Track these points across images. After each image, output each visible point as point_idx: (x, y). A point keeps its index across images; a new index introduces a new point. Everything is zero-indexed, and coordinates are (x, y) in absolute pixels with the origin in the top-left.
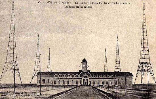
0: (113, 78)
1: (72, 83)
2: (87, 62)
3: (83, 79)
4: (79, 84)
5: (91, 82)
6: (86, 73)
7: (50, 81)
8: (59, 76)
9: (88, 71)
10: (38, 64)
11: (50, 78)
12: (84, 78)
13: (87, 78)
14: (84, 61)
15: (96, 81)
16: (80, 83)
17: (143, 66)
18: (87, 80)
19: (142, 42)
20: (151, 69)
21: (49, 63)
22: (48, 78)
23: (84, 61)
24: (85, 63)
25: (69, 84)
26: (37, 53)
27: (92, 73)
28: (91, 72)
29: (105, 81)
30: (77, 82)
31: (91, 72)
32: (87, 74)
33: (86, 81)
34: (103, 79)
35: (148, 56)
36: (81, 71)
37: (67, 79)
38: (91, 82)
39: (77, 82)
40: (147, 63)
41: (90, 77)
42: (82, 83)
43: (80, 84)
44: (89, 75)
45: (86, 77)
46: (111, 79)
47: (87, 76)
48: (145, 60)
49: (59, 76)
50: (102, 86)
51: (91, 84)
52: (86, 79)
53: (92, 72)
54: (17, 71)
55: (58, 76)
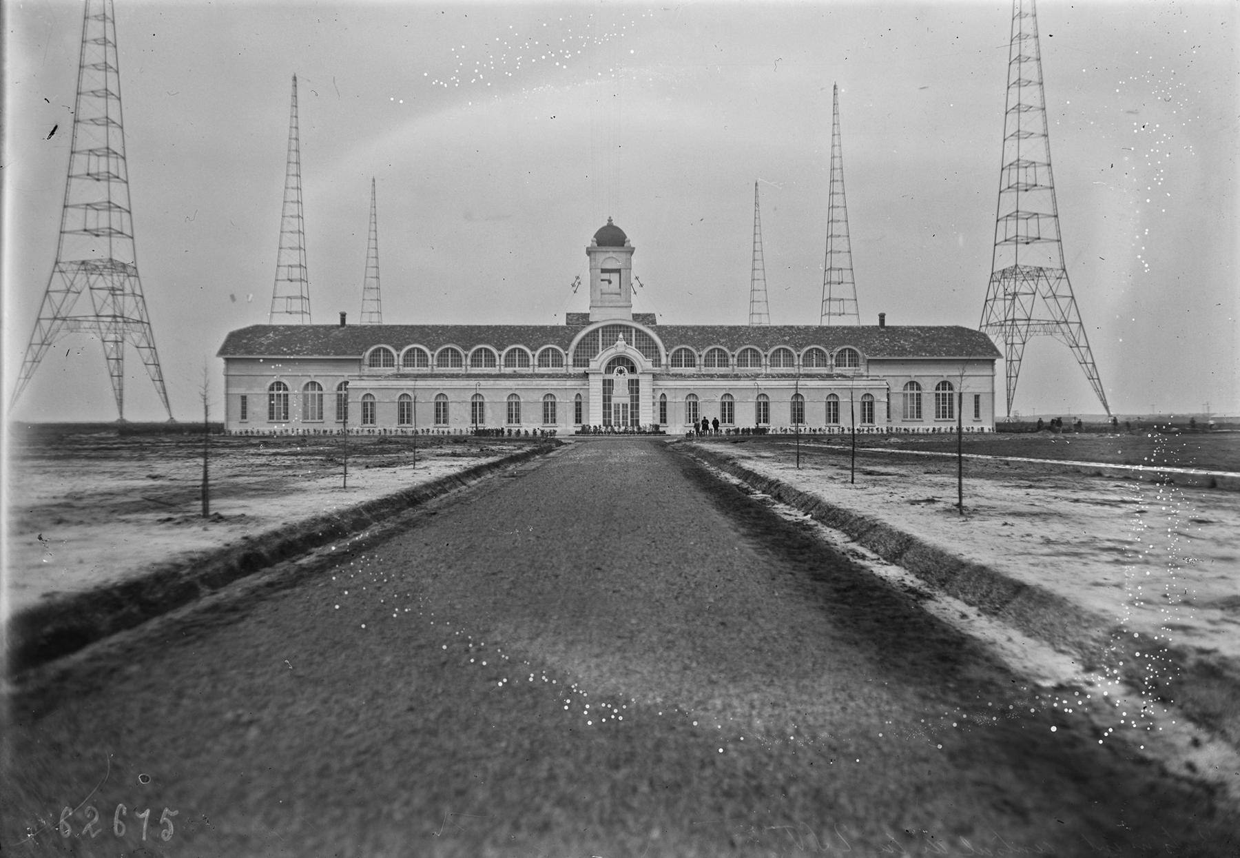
0: (837, 370)
1: (514, 413)
2: (631, 251)
3: (596, 384)
4: (565, 427)
5: (663, 405)
6: (626, 329)
7: (330, 403)
8: (408, 361)
9: (636, 317)
10: (294, 289)
11: (329, 379)
12: (609, 369)
13: (633, 370)
14: (611, 238)
15: (451, 396)
16: (571, 415)
17: (1015, 294)
18: (634, 386)
19: (1011, 130)
20: (1073, 318)
21: (291, 240)
22: (313, 373)
23: (611, 238)
24: (610, 258)
25: (489, 425)
26: (374, 264)
27: (672, 334)
28: (660, 322)
29: (459, 394)
30: (549, 412)
31: (660, 322)
32: (629, 343)
33: (621, 395)
34: (762, 383)
35: (1048, 229)
36: (587, 315)
37: (472, 383)
38: (663, 405)
39: (549, 412)
40: (1048, 273)
41: (657, 362)
42: (595, 418)
43: (578, 420)
44: (649, 349)
45: (621, 362)
46: (829, 377)
47: (633, 353)
48: (1030, 257)
49: (408, 361)
50: (757, 437)
51: (663, 419)
52: (621, 381)
53: (664, 328)
54: (136, 336)
55: (399, 356)
